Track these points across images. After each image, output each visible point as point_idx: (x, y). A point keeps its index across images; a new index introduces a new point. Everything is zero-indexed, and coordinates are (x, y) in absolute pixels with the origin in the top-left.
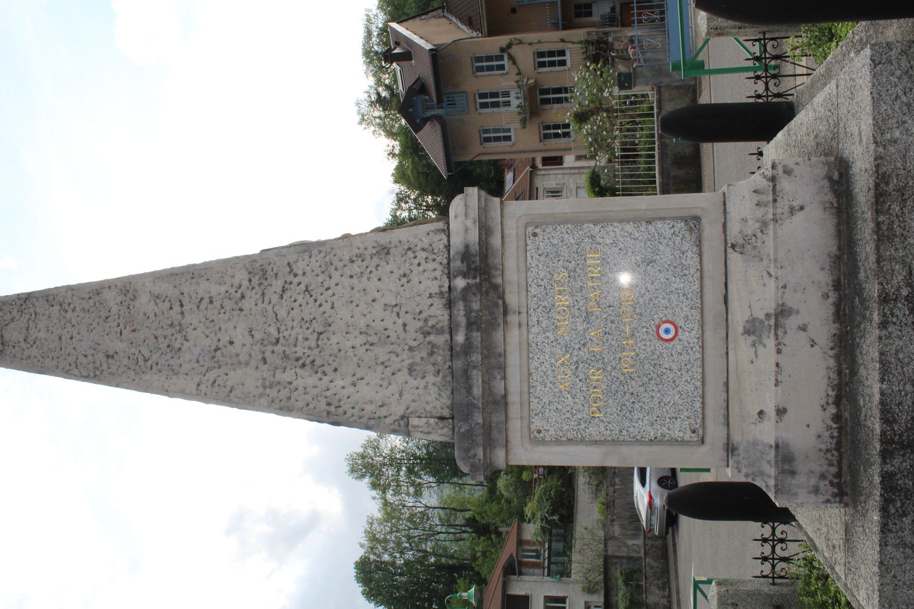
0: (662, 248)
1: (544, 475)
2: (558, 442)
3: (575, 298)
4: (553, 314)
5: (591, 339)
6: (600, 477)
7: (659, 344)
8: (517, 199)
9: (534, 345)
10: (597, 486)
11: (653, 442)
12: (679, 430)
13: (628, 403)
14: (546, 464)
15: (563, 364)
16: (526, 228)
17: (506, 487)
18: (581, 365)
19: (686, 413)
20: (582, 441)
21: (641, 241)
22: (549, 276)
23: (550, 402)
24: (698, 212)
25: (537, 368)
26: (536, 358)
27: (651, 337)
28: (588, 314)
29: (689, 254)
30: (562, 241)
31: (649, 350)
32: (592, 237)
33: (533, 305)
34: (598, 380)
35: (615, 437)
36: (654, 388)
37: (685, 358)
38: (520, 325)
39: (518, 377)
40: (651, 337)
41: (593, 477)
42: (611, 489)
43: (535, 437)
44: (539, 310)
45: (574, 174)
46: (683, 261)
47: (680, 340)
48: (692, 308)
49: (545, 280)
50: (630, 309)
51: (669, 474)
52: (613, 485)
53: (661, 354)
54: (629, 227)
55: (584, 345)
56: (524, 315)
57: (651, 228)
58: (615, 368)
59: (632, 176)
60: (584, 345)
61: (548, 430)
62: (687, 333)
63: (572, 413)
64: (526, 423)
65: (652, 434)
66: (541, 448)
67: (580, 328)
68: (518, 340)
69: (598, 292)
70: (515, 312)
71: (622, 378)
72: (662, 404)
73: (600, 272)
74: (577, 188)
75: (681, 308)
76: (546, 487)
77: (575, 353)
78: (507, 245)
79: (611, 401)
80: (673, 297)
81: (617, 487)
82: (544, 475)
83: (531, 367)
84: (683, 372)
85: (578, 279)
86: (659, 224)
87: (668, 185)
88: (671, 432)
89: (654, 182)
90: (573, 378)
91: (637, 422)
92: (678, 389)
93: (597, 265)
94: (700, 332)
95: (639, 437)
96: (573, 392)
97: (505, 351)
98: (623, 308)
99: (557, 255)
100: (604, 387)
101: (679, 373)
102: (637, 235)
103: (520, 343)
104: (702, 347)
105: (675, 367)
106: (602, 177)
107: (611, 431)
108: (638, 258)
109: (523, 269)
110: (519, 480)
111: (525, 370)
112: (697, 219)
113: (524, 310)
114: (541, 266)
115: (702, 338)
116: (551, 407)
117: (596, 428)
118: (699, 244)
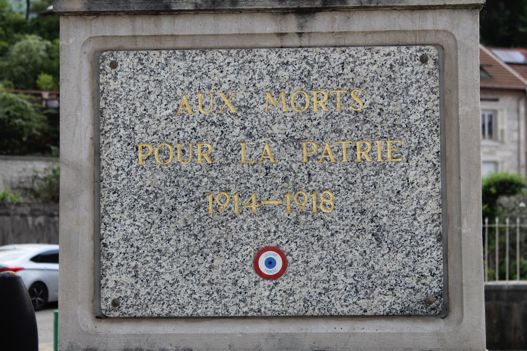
0: (400, 256)
1: (47, 108)
2: (97, 94)
3: (322, 121)
4: (298, 87)
5: (258, 145)
6: (46, 195)
7: (251, 250)
8: (481, 68)
9: (249, 57)
10: (32, 190)
11: (98, 239)
12: (118, 280)
13: (158, 202)
14: (62, 112)
15: (220, 102)
16: (436, 45)
17: (27, 49)
18: (218, 130)
19: (143, 292)
20: (98, 132)
21: (411, 225)
22: (357, 81)
23: (160, 82)
24: (455, 314)
25: (213, 61)
26: (231, 59)
27: (261, 238)
28: (297, 142)
29: (390, 299)
30: (413, 103)
31: (242, 235)
32: (419, 150)
33: (312, 54)
34: (195, 156)
35: (106, 183)
36: (182, 243)
37: (229, 290)
38: (281, 35)
39: (199, 32)
40: (261, 238)
41: (44, 184)
42: (26, 210)
43: (104, 58)
44: (304, 65)
45: (519, 159)
46: (378, 290)
47: (256, 283)
48: (305, 301)
49: (351, 75)
50: (304, 206)
51: (51, 299)
52: (34, 214)
53: (235, 254)
54: (432, 207)
55: (250, 135)
56: (296, 41)
57: (431, 241)
58: (213, 183)
59: (513, 245)
60: (250, 135)
61: (115, 78)
62: (267, 293)
63: (143, 116)
64: (129, 45)
65: (112, 240)
66: (86, 68)
67: (276, 129)
68: (257, 31)
69: (332, 157)
70: (301, 26)
71: (197, 194)
72: (157, 255)
73: (364, 160)
74: (496, 163)
75: (305, 285)
76: (26, 110)
77: (237, 122)
78: (408, 14)
79: (162, 176)
80: (322, 273)
81: (30, 219)
82: (47, 108)
83: (215, 52)
84: (208, 288)
85: (353, 127)
86: (437, 254)
87: (498, 298)
88: (114, 269)
89: (502, 277)
90: (198, 119)
91: (129, 216)
92: (180, 278)
93: (374, 156)
94: (269, 313)
95: (106, 219)
96: (176, 118)
97: (240, 11)
98: (306, 196)
99: (391, 95)
100: (184, 165)
101: (205, 281)
102: (421, 219)
103: (252, 35)
104: (245, 317)
105: (215, 274)
106: (513, 199)
107: (116, 177)
108: (385, 219)
109: (370, 39)
110: (38, 70)
111: (211, 43)
112: (444, 313)
113: (305, 41)
114: (374, 68)
115: (260, 317)
116: (152, 84)
117: (119, 153)
118: (406, 314)
